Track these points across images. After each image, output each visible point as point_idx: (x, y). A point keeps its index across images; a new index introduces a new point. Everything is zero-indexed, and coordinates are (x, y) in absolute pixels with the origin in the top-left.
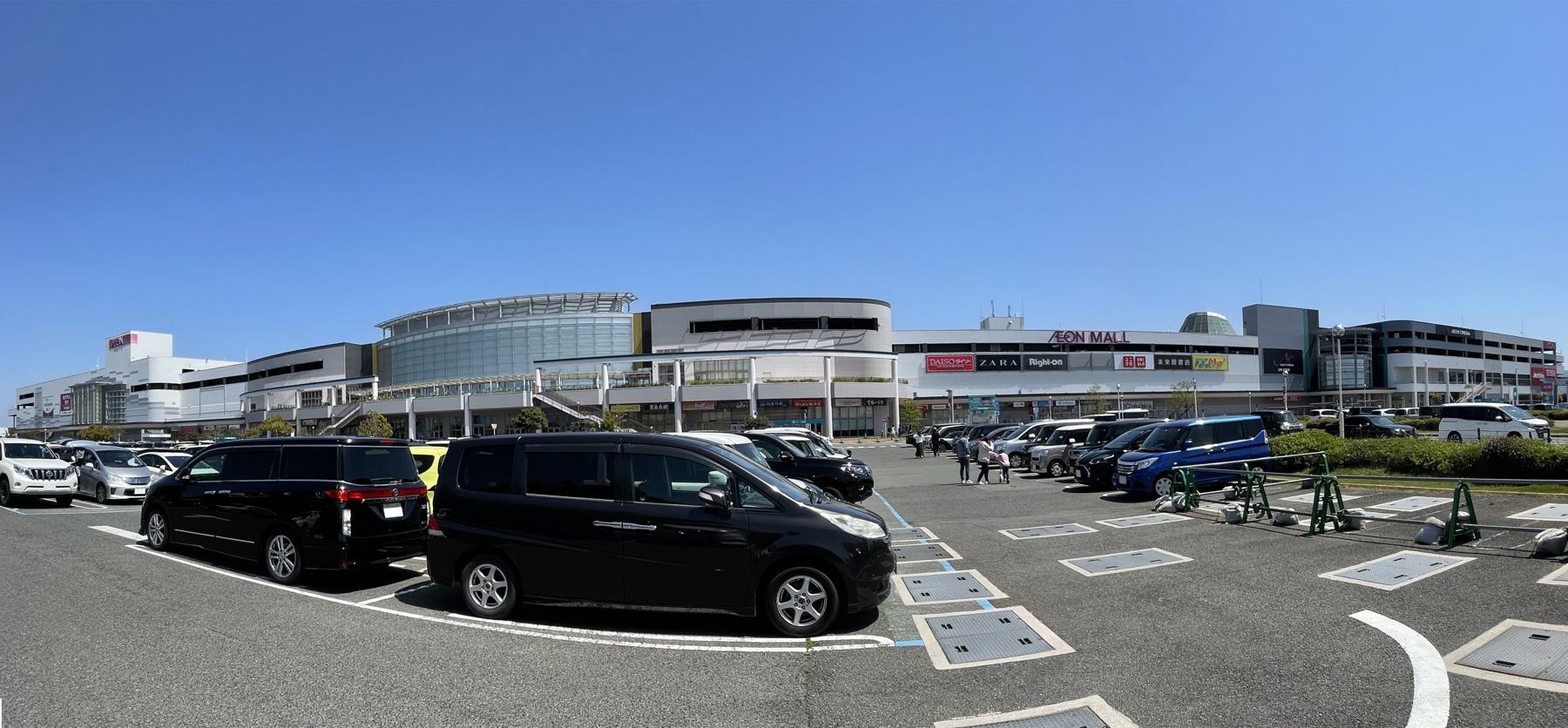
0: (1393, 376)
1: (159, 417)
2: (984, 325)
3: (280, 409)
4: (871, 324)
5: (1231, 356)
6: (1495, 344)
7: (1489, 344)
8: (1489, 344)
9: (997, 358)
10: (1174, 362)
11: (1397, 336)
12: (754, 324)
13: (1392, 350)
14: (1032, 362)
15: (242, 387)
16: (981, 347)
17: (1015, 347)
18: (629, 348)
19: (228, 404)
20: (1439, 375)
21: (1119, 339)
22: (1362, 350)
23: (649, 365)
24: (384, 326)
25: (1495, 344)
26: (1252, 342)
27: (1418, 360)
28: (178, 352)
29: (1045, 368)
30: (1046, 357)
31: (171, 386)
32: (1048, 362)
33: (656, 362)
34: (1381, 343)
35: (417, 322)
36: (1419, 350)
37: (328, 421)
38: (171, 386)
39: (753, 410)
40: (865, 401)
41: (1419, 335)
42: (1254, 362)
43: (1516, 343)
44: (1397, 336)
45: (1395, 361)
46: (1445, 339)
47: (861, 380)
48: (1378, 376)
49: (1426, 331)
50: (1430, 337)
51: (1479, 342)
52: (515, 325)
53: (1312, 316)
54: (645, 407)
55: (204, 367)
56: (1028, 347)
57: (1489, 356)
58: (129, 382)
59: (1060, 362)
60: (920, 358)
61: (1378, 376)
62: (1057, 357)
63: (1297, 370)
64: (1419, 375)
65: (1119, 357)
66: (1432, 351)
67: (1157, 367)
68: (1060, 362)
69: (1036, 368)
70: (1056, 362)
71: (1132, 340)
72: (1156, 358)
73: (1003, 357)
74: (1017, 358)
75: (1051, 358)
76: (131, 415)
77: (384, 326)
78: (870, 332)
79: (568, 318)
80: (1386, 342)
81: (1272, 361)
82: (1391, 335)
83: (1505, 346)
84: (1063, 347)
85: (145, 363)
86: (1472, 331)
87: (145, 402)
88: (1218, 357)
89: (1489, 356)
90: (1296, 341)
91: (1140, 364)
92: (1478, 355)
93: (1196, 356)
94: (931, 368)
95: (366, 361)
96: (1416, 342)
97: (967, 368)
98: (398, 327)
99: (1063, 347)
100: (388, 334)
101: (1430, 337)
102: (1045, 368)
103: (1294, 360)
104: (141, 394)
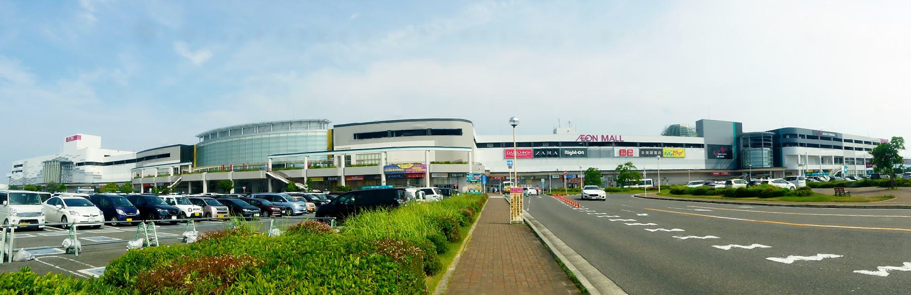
0: (787, 162)
1: (90, 180)
2: (555, 132)
3: (149, 176)
4: (458, 132)
5: (688, 149)
6: (850, 141)
7: (846, 141)
8: (846, 141)
9: (545, 150)
10: (651, 153)
11: (788, 137)
12: (389, 134)
13: (785, 145)
14: (567, 152)
15: (134, 165)
16: (551, 144)
17: (557, 144)
18: (325, 148)
19: (123, 174)
20: (814, 158)
21: (618, 139)
22: (766, 145)
23: (333, 156)
24: (200, 136)
25: (850, 141)
26: (700, 141)
27: (800, 151)
28: (104, 146)
29: (574, 156)
30: (574, 150)
31: (97, 164)
32: (575, 153)
33: (336, 154)
34: (780, 140)
35: (214, 134)
36: (802, 145)
37: (169, 184)
38: (97, 164)
39: (384, 178)
40: (450, 174)
41: (803, 136)
42: (701, 153)
43: (864, 140)
44: (788, 137)
45: (787, 151)
46: (816, 139)
47: (448, 163)
48: (777, 160)
49: (806, 134)
50: (809, 137)
51: (840, 140)
52: (309, 134)
53: (738, 126)
54: (326, 178)
55: (116, 155)
56: (564, 144)
57: (847, 148)
58: (75, 161)
59: (583, 152)
60: (501, 150)
61: (777, 160)
62: (581, 150)
63: (729, 156)
64: (802, 159)
65: (617, 149)
66: (809, 145)
67: (641, 156)
68: (583, 152)
69: (568, 156)
70: (580, 153)
71: (626, 140)
72: (641, 150)
73: (550, 150)
74: (557, 150)
75: (578, 150)
76: (76, 178)
77: (200, 136)
78: (78, 141)
79: (293, 133)
80: (781, 141)
81: (713, 151)
82: (785, 136)
83: (856, 142)
84: (584, 144)
85: (84, 151)
86: (836, 134)
87: (83, 172)
88: (679, 149)
89: (847, 148)
90: (726, 138)
91: (630, 154)
92: (840, 148)
93: (666, 149)
94: (508, 156)
95: (187, 153)
96: (799, 140)
97: (528, 157)
98: (206, 136)
99: (584, 144)
100: (202, 140)
101: (809, 137)
102: (574, 156)
103: (727, 151)
104: (81, 168)
